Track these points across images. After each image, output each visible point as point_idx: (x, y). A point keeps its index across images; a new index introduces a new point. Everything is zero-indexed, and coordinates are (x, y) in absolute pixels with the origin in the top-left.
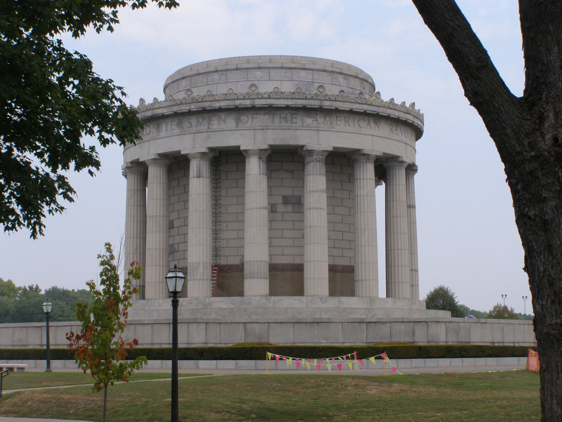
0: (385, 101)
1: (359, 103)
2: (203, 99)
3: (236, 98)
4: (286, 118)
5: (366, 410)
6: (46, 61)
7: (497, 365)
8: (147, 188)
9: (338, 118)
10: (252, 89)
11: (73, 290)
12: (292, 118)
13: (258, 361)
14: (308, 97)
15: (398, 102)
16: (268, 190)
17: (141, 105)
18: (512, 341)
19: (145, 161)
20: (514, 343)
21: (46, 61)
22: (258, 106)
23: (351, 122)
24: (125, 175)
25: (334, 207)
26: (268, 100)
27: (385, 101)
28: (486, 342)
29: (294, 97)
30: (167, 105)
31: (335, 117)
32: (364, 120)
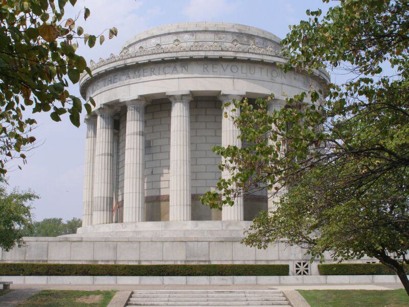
1: (156, 54)
3: (220, 49)
4: (111, 80)
7: (257, 284)
9: (145, 71)
12: (114, 79)
13: (259, 277)
15: (105, 58)
18: (138, 259)
20: (140, 261)
23: (156, 71)
25: (196, 174)
31: (142, 71)
32: (170, 67)
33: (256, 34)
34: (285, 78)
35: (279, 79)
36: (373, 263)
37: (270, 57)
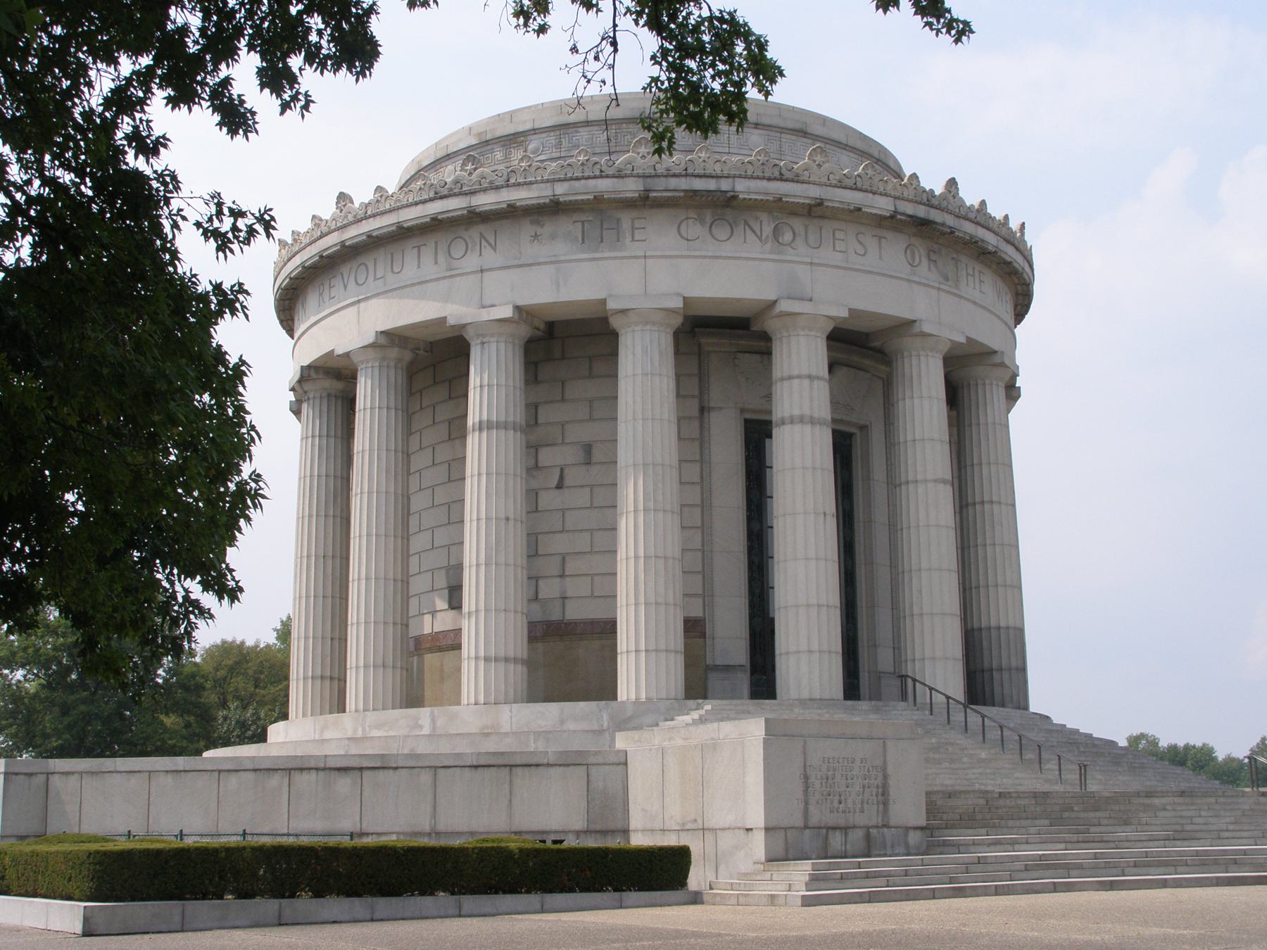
0: (968, 204)
2: (508, 181)
3: (777, 174)
6: (96, 173)
10: (638, 150)
11: (243, 643)
14: (787, 175)
15: (996, 211)
16: (951, 436)
17: (341, 211)
19: (464, 326)
21: (96, 173)
26: (683, 179)
27: (968, 204)
30: (410, 200)
33: (528, 126)
34: (494, 249)
35: (472, 261)
36: (555, 842)
37: (420, 207)
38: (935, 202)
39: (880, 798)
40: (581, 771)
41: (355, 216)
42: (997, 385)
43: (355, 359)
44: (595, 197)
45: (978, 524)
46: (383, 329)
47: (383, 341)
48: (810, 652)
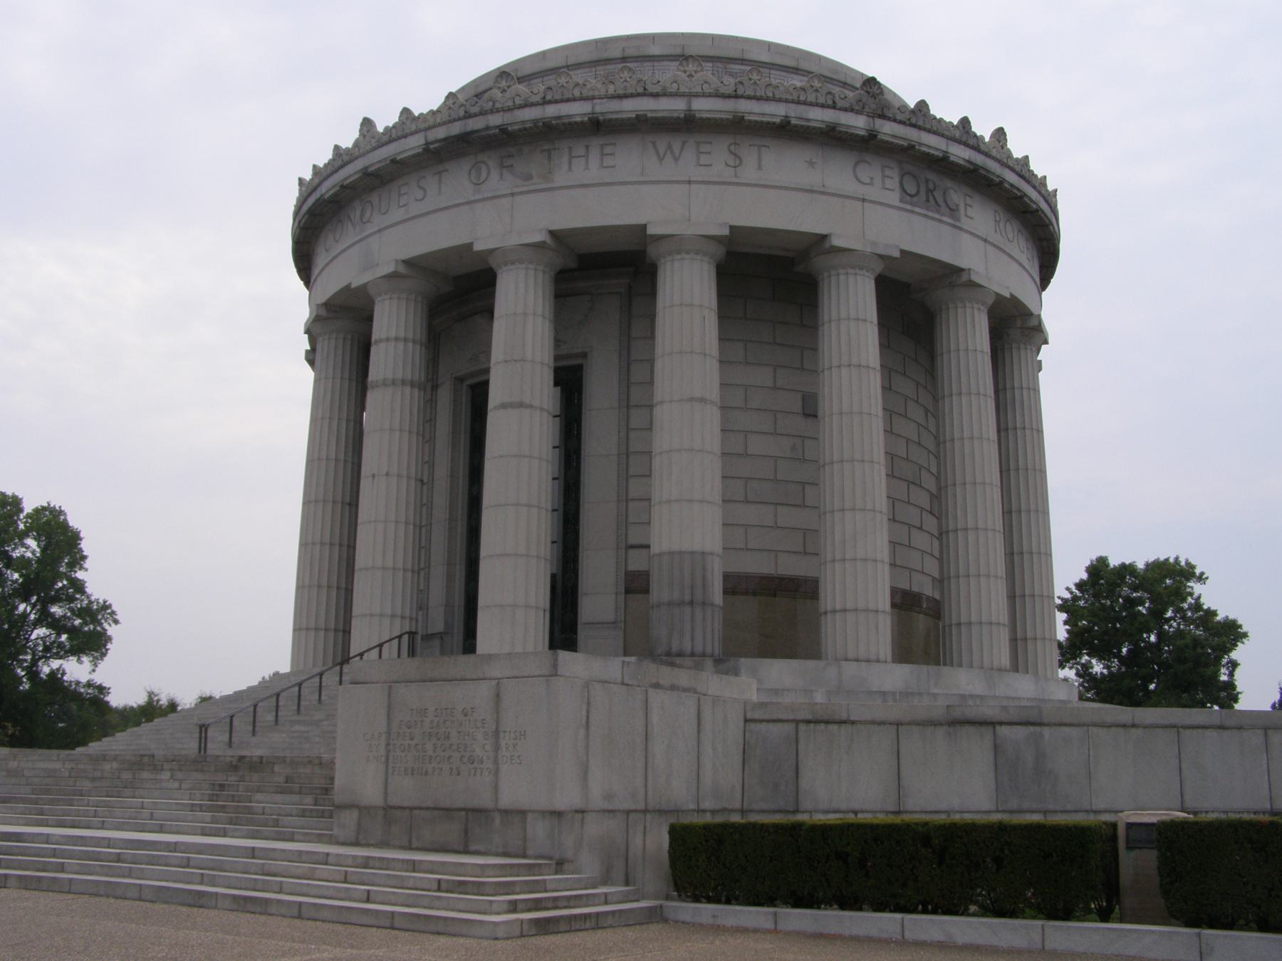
5: (214, 792)
8: (365, 413)
15: (1037, 168)
22: (705, 115)
24: (311, 358)
28: (916, 812)
29: (802, 98)
38: (982, 147)
39: (392, 742)
40: (1176, 729)
41: (378, 141)
42: (1032, 349)
43: (372, 292)
44: (637, 115)
45: (1030, 483)
46: (403, 259)
47: (402, 269)
48: (988, 576)
